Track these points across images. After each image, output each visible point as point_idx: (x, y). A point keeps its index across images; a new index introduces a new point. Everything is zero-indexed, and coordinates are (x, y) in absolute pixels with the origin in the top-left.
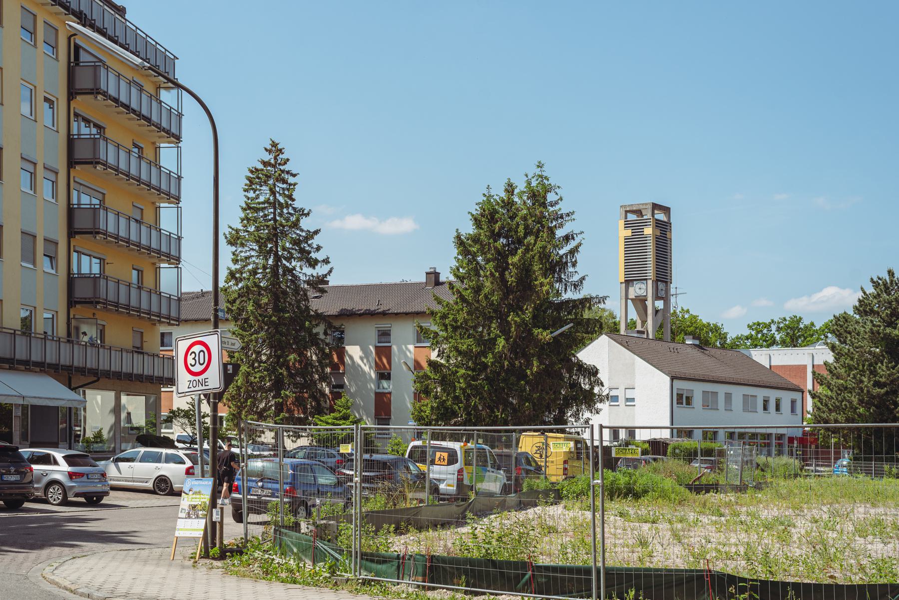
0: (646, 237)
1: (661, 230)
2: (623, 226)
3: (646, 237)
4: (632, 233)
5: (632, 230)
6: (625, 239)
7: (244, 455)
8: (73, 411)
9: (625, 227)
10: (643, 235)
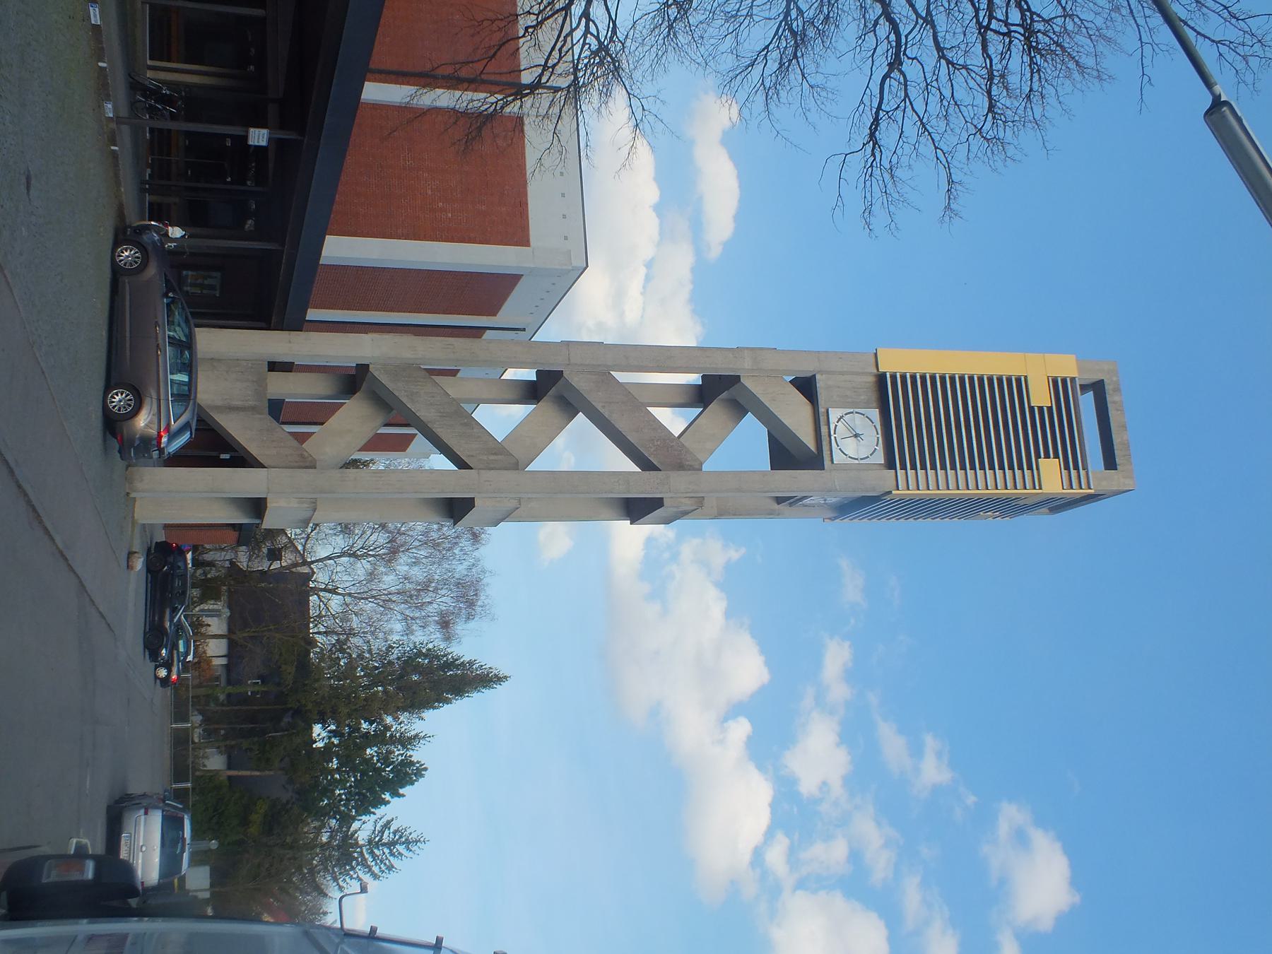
0: (1030, 468)
1: (1038, 456)
2: (1061, 374)
3: (1030, 468)
4: (1041, 409)
5: (1050, 409)
6: (1018, 380)
7: (951, 469)
8: (1023, 379)
9: (1055, 381)
10: (1038, 456)
